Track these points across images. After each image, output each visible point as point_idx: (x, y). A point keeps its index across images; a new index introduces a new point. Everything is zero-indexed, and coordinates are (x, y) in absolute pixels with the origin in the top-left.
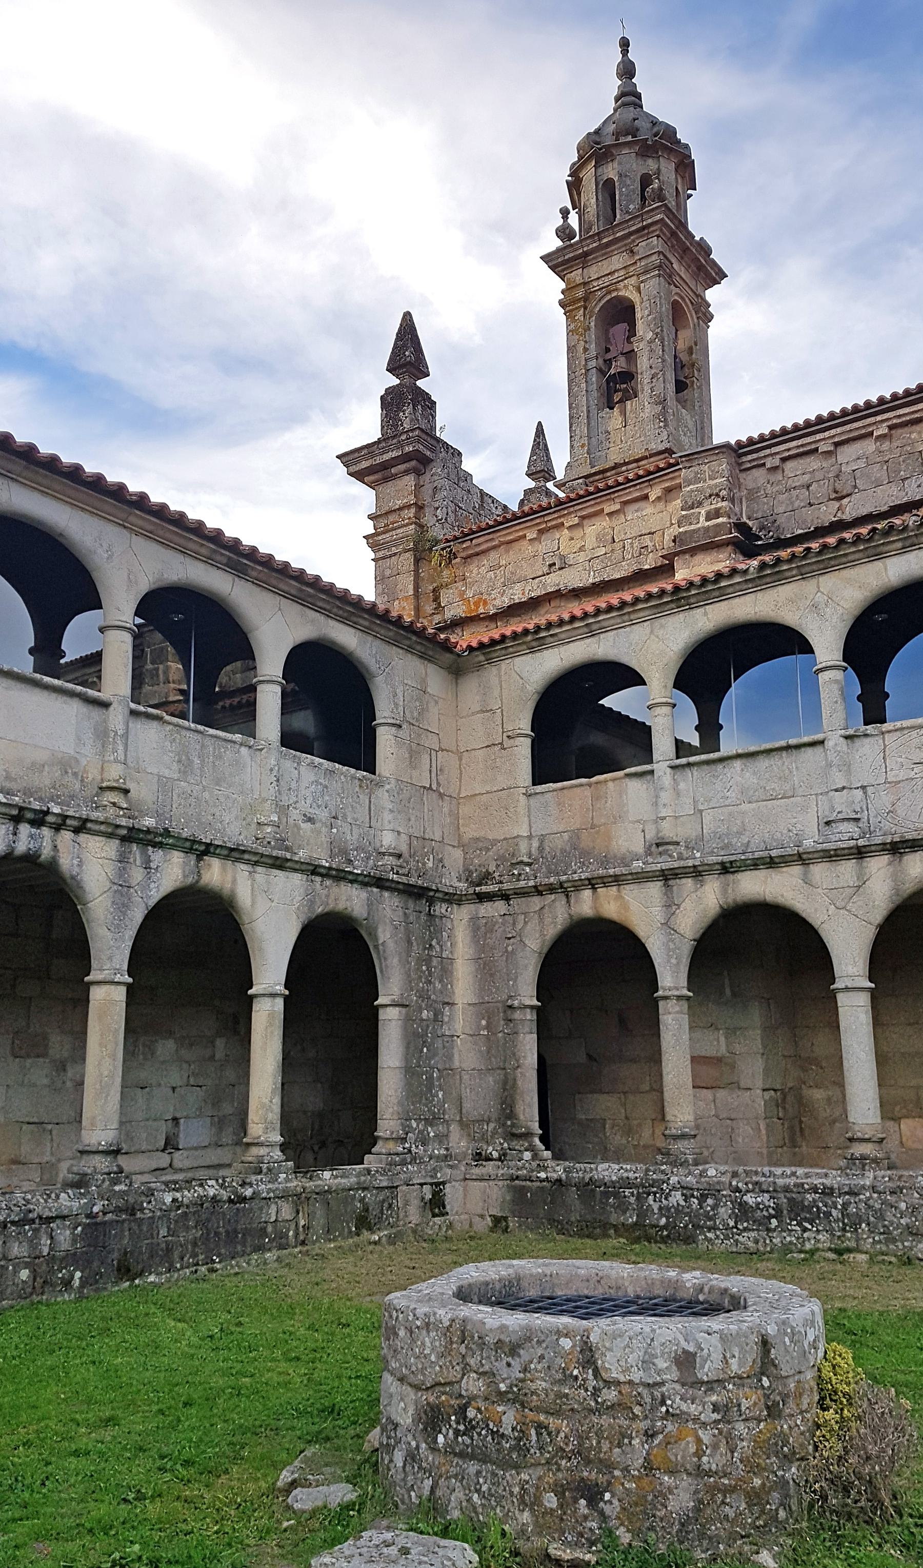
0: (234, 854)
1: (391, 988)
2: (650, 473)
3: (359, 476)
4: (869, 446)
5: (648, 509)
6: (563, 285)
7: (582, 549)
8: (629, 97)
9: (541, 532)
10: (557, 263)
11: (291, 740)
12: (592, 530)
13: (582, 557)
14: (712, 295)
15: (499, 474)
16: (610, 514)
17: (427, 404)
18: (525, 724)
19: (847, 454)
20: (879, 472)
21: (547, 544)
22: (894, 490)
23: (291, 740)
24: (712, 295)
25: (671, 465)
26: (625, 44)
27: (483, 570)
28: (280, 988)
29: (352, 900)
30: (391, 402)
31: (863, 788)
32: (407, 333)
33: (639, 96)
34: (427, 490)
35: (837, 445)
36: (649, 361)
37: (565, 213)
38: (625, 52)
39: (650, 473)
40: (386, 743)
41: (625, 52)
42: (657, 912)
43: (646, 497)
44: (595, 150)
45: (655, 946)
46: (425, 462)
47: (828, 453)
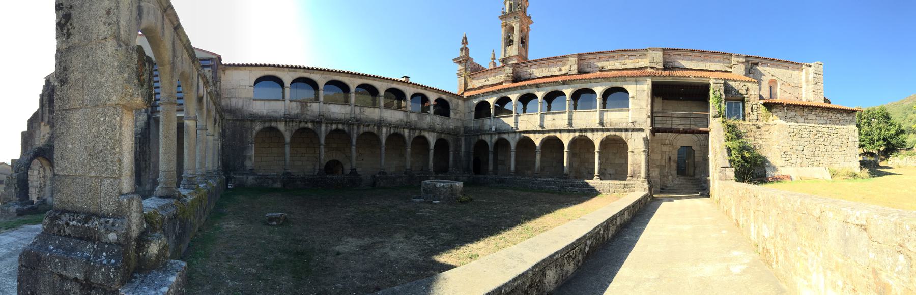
32: (465, 38)
36: (516, 37)
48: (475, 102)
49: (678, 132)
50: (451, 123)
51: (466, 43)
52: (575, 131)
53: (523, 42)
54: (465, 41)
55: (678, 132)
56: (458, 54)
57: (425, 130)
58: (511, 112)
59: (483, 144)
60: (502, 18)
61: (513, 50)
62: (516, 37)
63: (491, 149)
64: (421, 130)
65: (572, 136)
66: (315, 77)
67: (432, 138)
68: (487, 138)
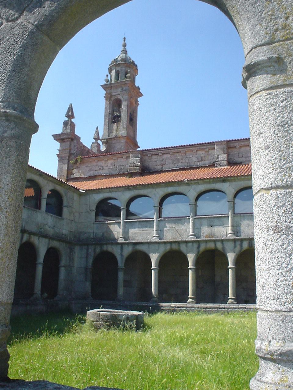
0: (34, 234)
1: (63, 262)
2: (123, 153)
3: (57, 140)
4: (169, 156)
5: (122, 160)
6: (105, 92)
7: (107, 166)
8: (125, 51)
9: (98, 161)
10: (104, 87)
11: (48, 211)
12: (110, 162)
13: (107, 168)
14: (139, 99)
15: (87, 141)
16: (114, 160)
17: (73, 126)
18: (94, 208)
19: (165, 156)
20: (170, 161)
21: (100, 163)
22: (173, 165)
23: (48, 211)
24: (139, 99)
25: (129, 152)
26: (125, 39)
27: (84, 167)
28: (42, 262)
29: (55, 244)
30: (65, 124)
31: (161, 230)
32: (70, 109)
33: (127, 52)
34: (72, 146)
35: (163, 154)
36: (124, 115)
37: (107, 76)
38: (124, 41)
39: (123, 153)
40: (65, 211)
41: (124, 41)
42: (119, 251)
43: (122, 157)
44: (115, 65)
45: (119, 258)
46: (72, 140)
47: (161, 155)
48: (98, 197)
49: (247, 55)
50: (65, 227)
51: (72, 116)
52: (165, 243)
53: (132, 119)
54: (70, 114)
55: (247, 55)
56: (59, 130)
57: (34, 234)
58: (118, 210)
59: (111, 257)
60: (104, 87)
61: (121, 130)
62: (124, 115)
63: (121, 264)
64: (31, 233)
65: (163, 249)
66: (41, 181)
67: (42, 247)
68: (116, 250)
